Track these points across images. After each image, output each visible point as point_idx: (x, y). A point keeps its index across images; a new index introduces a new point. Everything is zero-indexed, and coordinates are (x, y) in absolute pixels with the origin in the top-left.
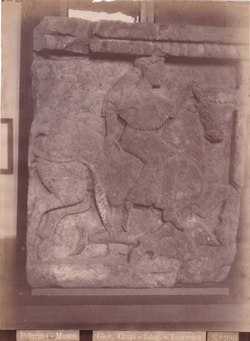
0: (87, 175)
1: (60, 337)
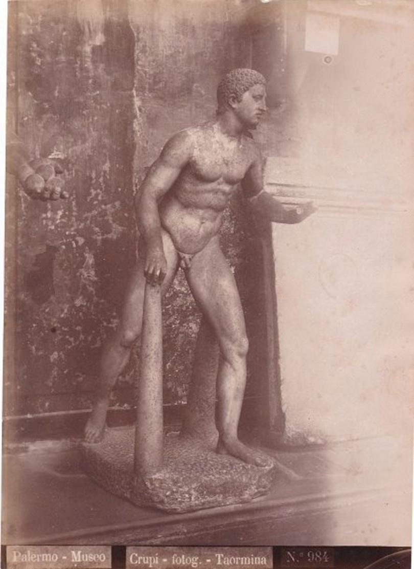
0: (95, 145)
1: (78, 559)
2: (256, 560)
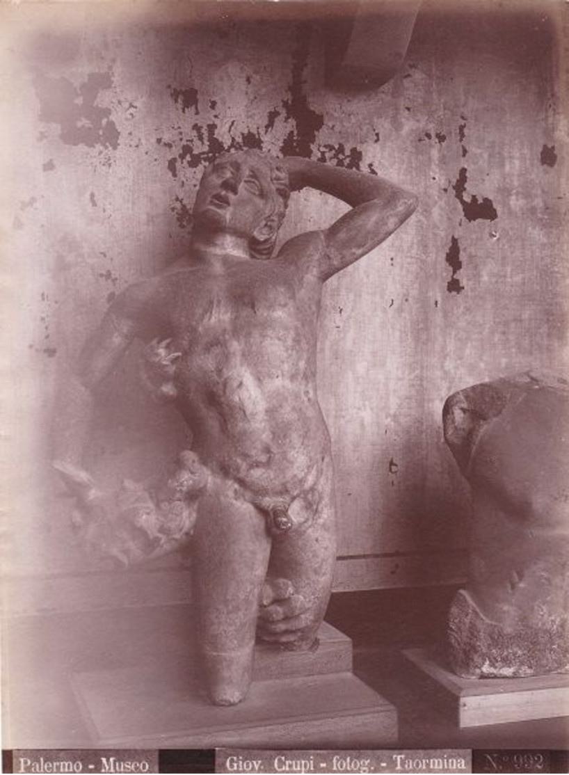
2: (446, 763)
